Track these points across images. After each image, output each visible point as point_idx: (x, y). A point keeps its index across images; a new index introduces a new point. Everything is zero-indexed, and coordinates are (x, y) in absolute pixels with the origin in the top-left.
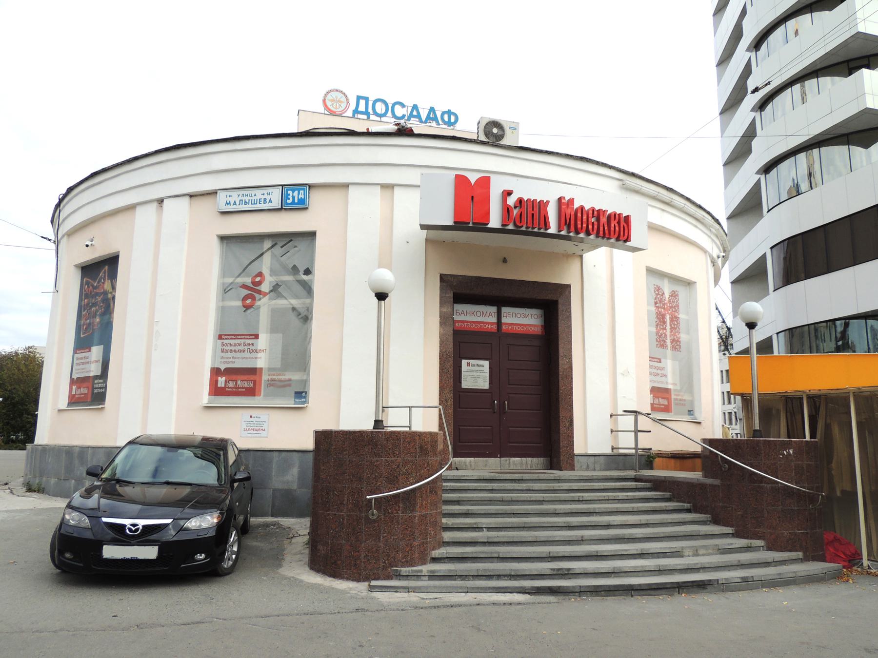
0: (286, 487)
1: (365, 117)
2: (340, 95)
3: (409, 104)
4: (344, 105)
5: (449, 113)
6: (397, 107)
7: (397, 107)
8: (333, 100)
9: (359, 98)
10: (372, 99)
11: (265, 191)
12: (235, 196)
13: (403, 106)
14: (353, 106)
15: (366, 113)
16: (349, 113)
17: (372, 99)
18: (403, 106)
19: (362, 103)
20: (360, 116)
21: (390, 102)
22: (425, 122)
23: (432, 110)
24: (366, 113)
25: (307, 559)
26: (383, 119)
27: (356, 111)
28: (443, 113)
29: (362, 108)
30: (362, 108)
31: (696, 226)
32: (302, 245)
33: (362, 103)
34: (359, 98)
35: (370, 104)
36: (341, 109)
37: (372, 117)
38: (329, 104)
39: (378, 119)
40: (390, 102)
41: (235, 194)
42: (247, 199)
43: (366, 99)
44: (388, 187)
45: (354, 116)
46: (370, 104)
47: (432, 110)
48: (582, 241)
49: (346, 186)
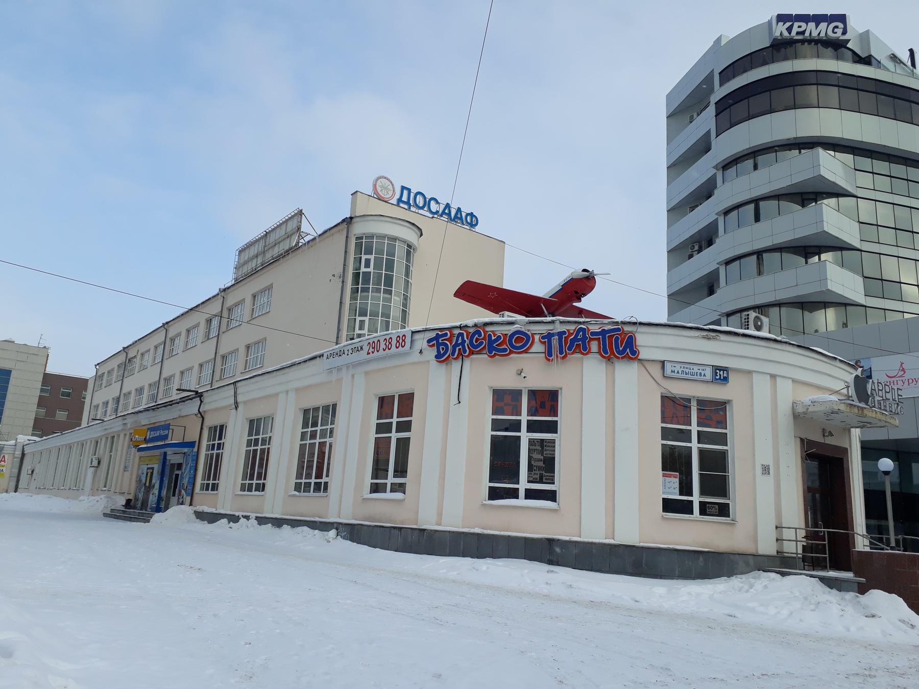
0: (843, 593)
1: (406, 207)
2: (390, 187)
3: (443, 201)
4: (391, 193)
5: (472, 215)
6: (432, 202)
7: (432, 202)
8: (381, 187)
9: (403, 188)
10: (414, 191)
11: (701, 368)
12: (678, 368)
13: (437, 202)
14: (397, 196)
15: (408, 203)
16: (394, 201)
17: (414, 191)
18: (437, 202)
19: (405, 192)
20: (402, 205)
21: (428, 197)
22: (454, 220)
23: (459, 210)
24: (408, 203)
25: (676, 288)
26: (421, 211)
27: (400, 200)
28: (467, 215)
29: (405, 198)
30: (405, 198)
31: (657, 334)
32: (531, 479)
33: (405, 192)
34: (403, 188)
35: (412, 195)
36: (388, 196)
37: (413, 209)
38: (379, 189)
39: (431, 216)
40: (428, 197)
41: (678, 366)
42: (687, 371)
43: (409, 190)
44: (773, 377)
45: (398, 205)
46: (412, 195)
47: (459, 210)
48: (137, 432)
49: (750, 372)
